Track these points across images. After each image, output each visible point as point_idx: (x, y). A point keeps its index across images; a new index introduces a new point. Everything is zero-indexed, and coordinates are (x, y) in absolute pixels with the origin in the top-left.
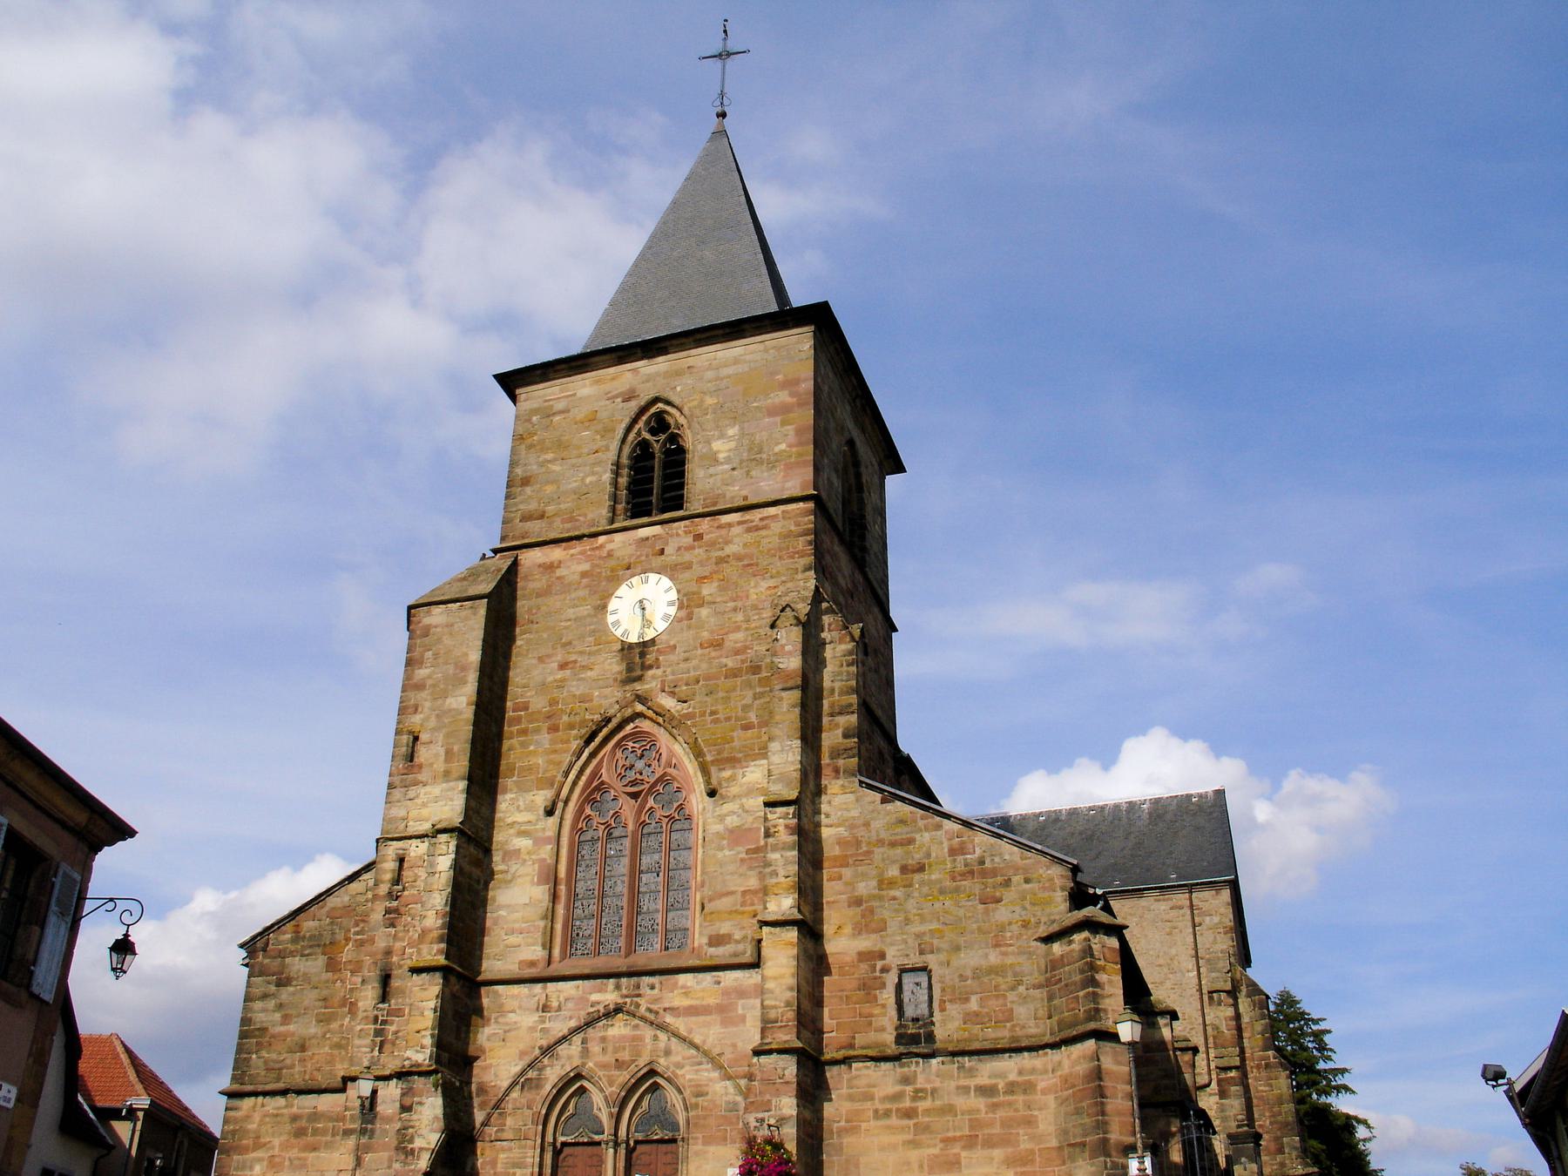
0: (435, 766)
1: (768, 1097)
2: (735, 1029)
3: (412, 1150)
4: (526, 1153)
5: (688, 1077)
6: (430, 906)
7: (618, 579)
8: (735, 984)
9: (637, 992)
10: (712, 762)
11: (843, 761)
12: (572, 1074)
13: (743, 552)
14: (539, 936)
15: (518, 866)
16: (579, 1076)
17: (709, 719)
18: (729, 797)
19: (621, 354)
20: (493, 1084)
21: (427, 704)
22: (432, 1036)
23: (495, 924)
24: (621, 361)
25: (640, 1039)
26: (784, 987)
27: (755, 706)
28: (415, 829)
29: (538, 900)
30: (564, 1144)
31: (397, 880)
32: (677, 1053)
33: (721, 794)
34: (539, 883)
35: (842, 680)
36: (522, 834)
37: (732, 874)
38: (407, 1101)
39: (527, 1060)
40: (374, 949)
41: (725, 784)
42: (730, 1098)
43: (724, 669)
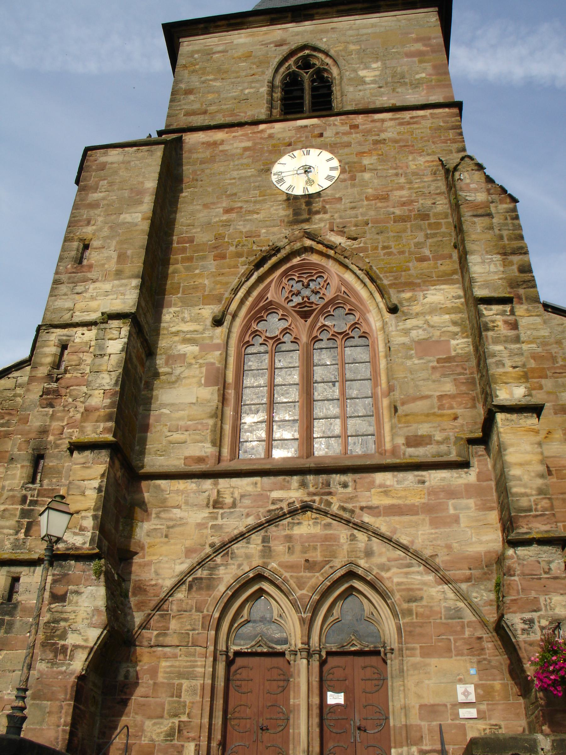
0: (106, 266)
1: (533, 594)
2: (448, 530)
3: (64, 649)
4: (196, 661)
5: (396, 580)
6: (97, 385)
7: (280, 152)
8: (442, 484)
9: (327, 490)
10: (391, 285)
11: (523, 290)
12: (251, 575)
13: (398, 137)
14: (208, 434)
15: (183, 369)
16: (260, 577)
17: (382, 252)
18: (412, 314)
19: (273, 16)
20: (153, 582)
21: (100, 219)
22: (95, 517)
23: (158, 421)
24: (273, 22)
25: (334, 538)
26: (533, 474)
27: (428, 244)
28: (81, 319)
29: (206, 400)
30: (238, 654)
31: (57, 365)
32: (380, 555)
33: (403, 312)
34: (207, 385)
35: (509, 230)
36: (186, 341)
37: (424, 380)
38: (60, 590)
39: (195, 558)
40: (27, 428)
41: (405, 304)
42: (451, 603)
43: (392, 216)
